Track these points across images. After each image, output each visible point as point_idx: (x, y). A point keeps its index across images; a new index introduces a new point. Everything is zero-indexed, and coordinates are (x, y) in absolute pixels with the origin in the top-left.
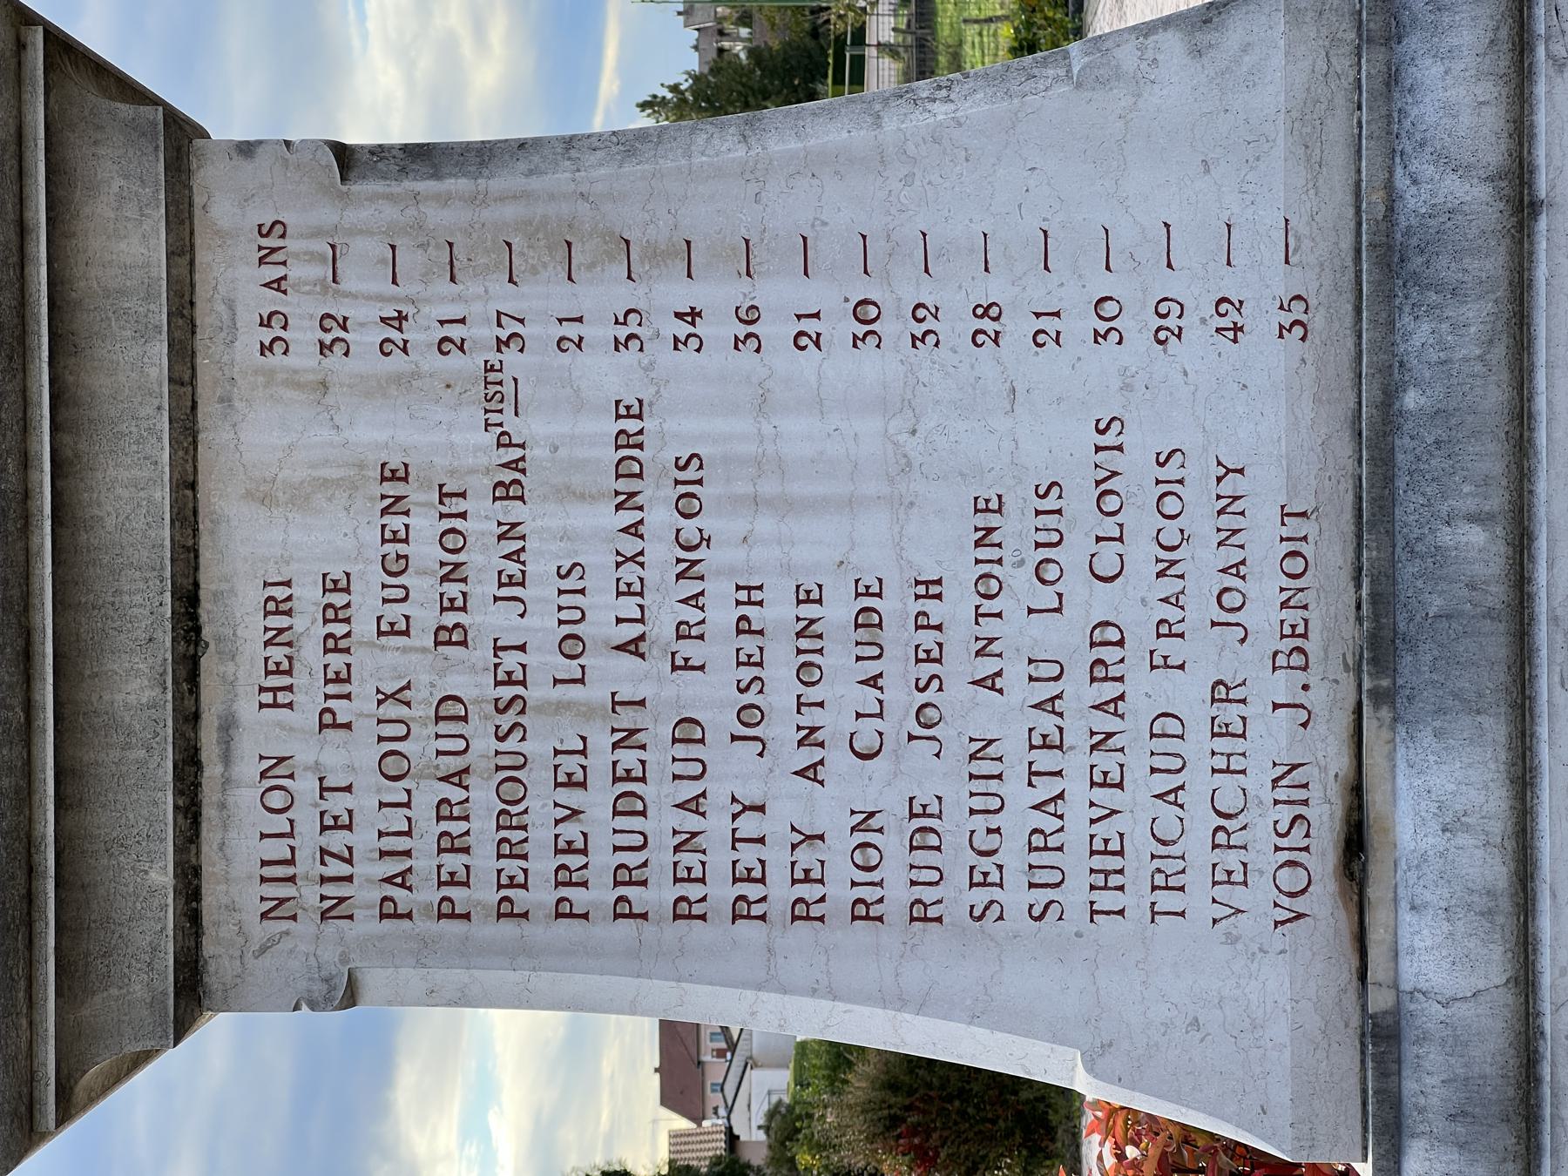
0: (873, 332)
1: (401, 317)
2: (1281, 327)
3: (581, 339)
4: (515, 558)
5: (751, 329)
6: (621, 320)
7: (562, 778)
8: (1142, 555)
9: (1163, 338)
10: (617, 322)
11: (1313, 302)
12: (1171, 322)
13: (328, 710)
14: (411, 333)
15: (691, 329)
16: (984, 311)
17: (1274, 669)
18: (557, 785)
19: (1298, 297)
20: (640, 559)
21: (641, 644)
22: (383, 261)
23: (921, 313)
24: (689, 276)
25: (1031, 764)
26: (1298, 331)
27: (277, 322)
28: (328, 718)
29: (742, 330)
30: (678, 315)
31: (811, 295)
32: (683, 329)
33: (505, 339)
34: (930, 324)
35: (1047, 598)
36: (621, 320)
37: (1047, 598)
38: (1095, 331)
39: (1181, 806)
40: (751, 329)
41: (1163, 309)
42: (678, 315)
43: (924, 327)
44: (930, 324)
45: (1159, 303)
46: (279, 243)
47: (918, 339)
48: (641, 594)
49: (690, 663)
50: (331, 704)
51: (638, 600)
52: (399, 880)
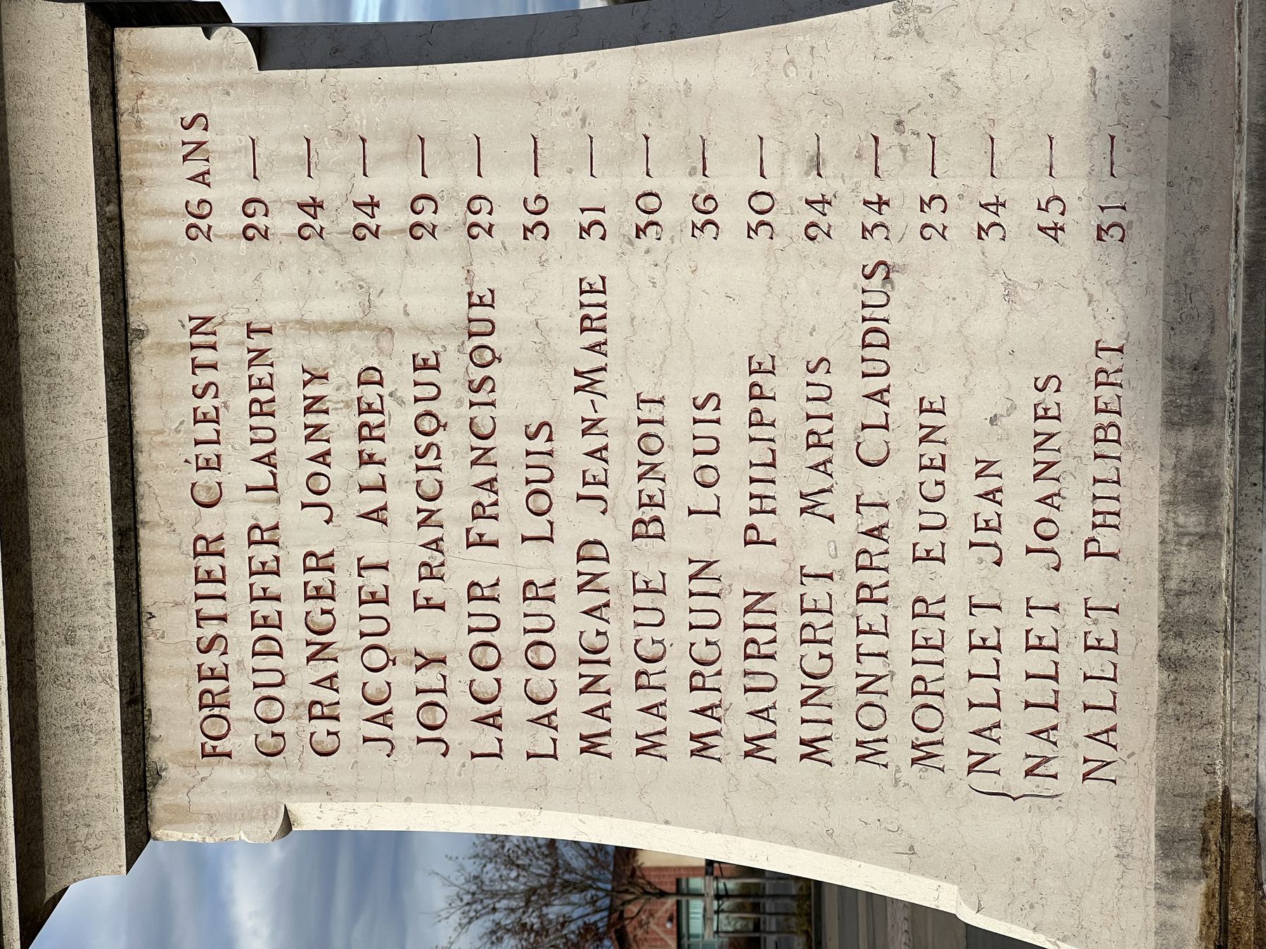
0: (542, 223)
1: (374, 204)
3: (491, 226)
4: (321, 459)
5: (652, 217)
6: (1043, 206)
8: (403, 502)
10: (1039, 208)
11: (1071, 202)
12: (483, 219)
13: (752, 527)
14: (383, 219)
21: (828, 465)
22: (300, 158)
24: (479, 175)
25: (858, 646)
27: (1056, 207)
28: (752, 534)
29: (531, 220)
31: (598, 189)
35: (539, 526)
36: (1043, 206)
37: (539, 526)
40: (652, 217)
41: (476, 205)
47: (697, 228)
49: (431, 602)
50: (755, 519)
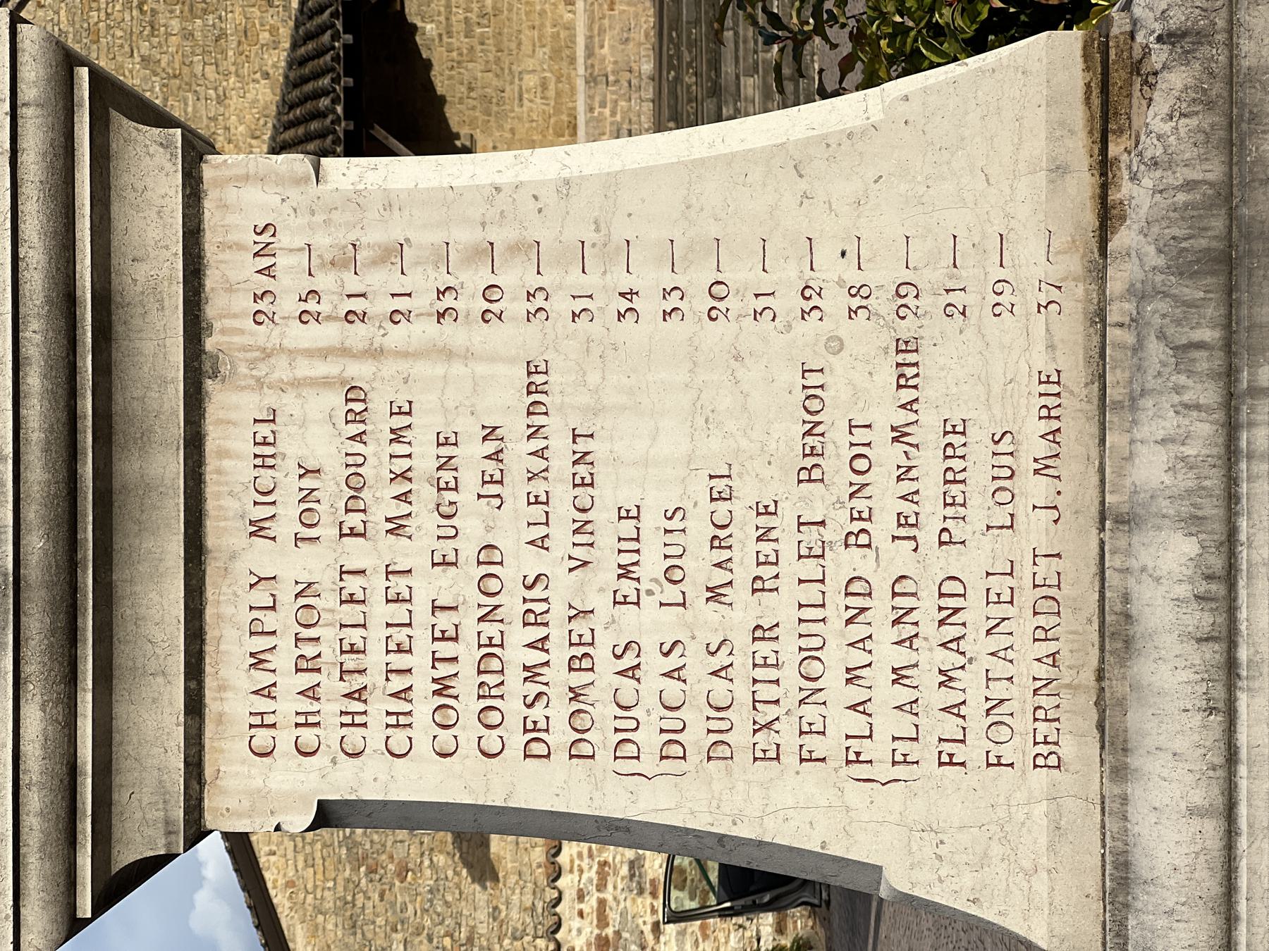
2: (529, 313)
6: (303, 298)
7: (438, 634)
9: (714, 317)
15: (630, 305)
16: (628, 295)
17: (988, 603)
18: (434, 639)
19: (541, 289)
20: (393, 476)
23: (807, 293)
26: (542, 315)
30: (622, 295)
32: (624, 305)
33: (807, 311)
34: (816, 301)
36: (303, 298)
38: (573, 312)
39: (964, 717)
42: (622, 295)
43: (811, 304)
44: (816, 301)
45: (899, 286)
46: (272, 240)
48: (547, 503)
51: (545, 508)
52: (356, 695)
